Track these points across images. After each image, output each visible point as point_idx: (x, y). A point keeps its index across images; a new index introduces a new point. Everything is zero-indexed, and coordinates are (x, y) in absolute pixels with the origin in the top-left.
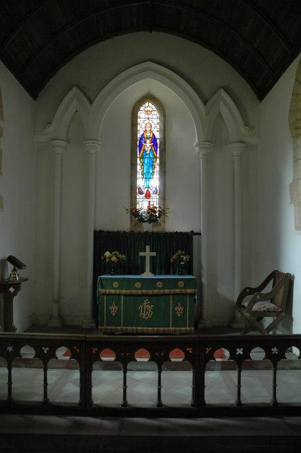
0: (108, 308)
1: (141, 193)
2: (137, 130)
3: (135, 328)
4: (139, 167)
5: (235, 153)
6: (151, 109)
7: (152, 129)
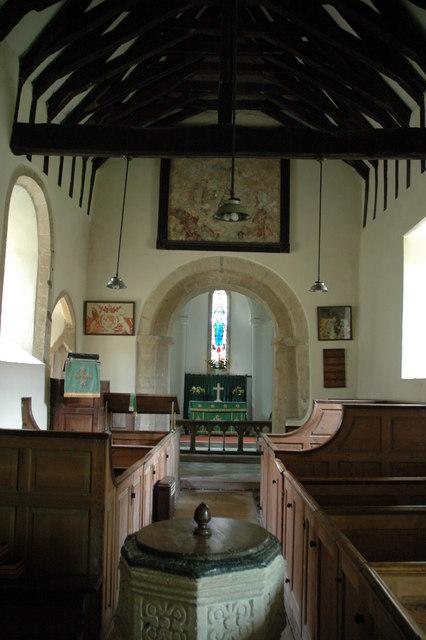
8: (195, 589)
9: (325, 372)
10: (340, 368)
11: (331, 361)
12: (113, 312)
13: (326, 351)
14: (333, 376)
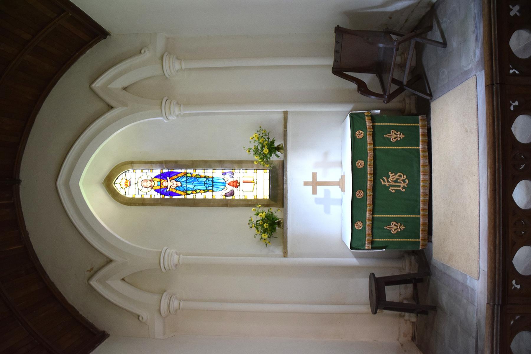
0: (393, 236)
1: (232, 193)
2: (151, 199)
3: (421, 198)
4: (199, 196)
5: (177, 113)
6: (124, 180)
7: (150, 178)
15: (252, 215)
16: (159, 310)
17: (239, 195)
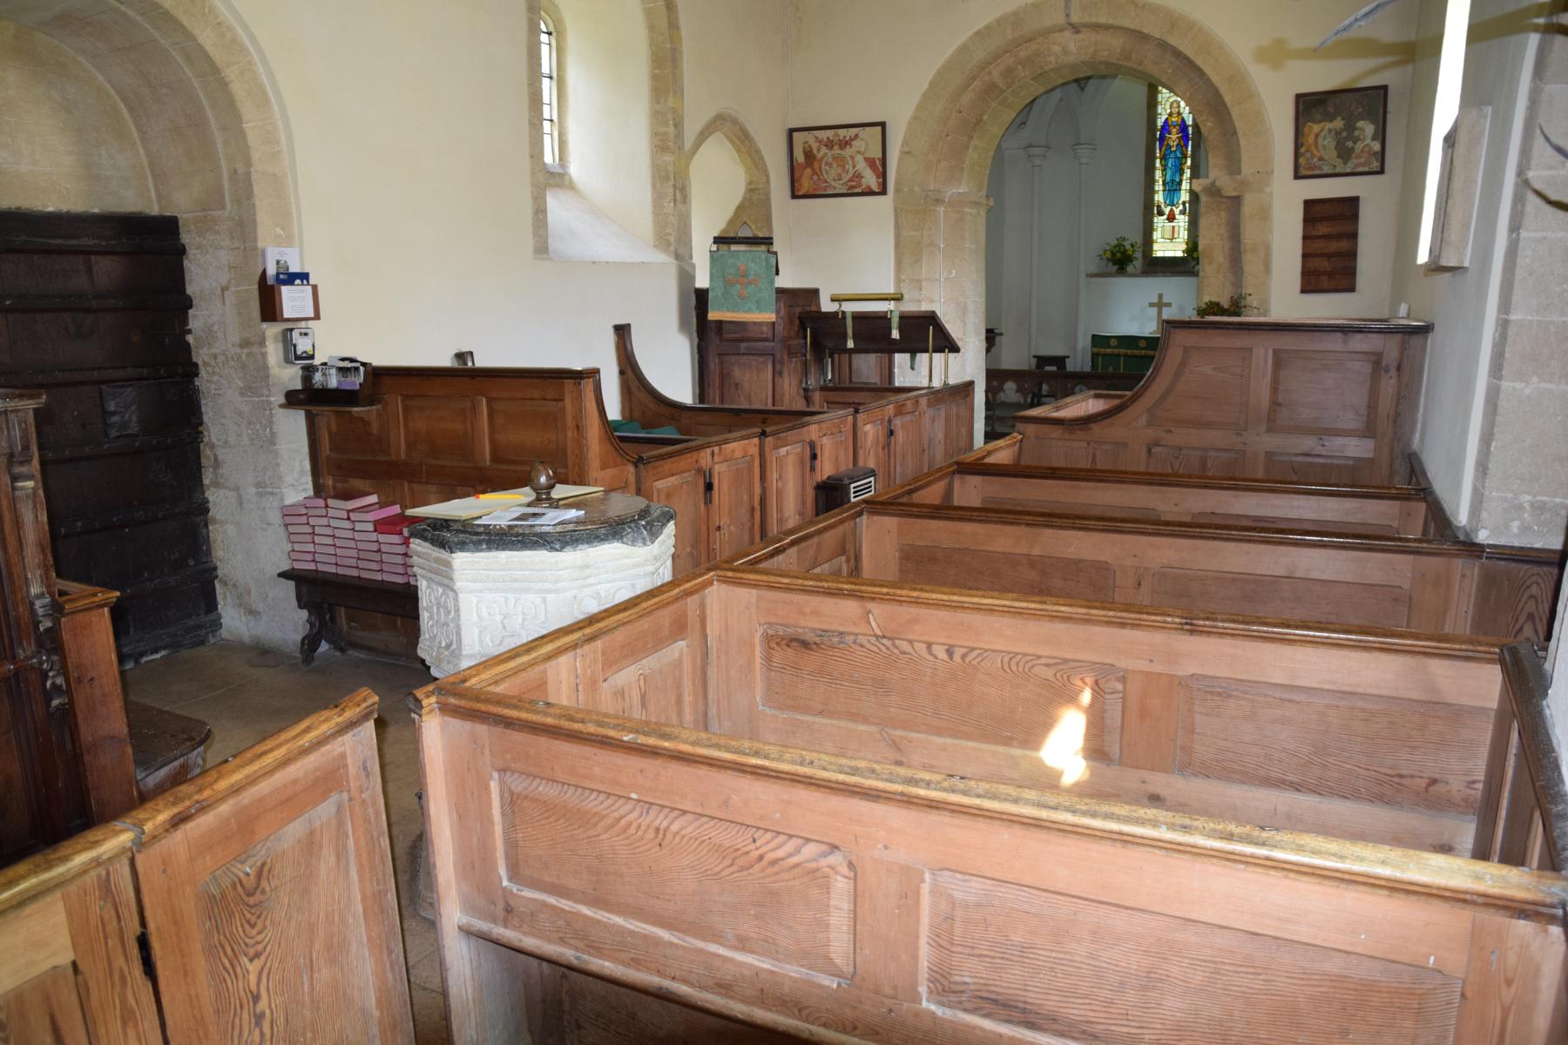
1: (1161, 213)
4: (1158, 174)
8: (448, 565)
9: (1305, 256)
10: (1344, 245)
11: (1323, 229)
12: (841, 148)
13: (1309, 204)
14: (1324, 264)
15: (1134, 237)
16: (1031, 146)
17: (1159, 222)
